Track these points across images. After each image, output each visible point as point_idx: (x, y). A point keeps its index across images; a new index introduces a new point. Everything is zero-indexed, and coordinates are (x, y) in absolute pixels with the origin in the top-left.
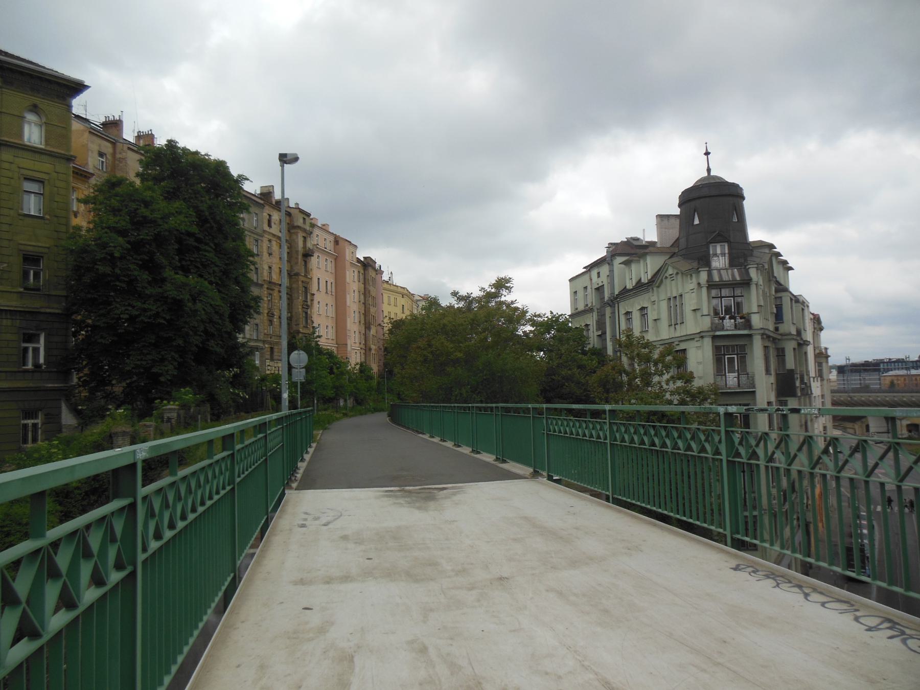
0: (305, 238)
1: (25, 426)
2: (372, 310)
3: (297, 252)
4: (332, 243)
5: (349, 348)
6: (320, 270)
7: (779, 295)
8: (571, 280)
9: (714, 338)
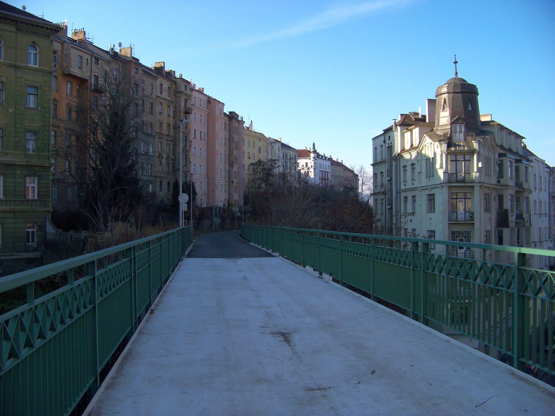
0: (186, 100)
1: (28, 232)
2: (235, 152)
3: (180, 110)
4: (206, 102)
5: (216, 182)
6: (197, 123)
7: (501, 158)
8: (373, 139)
9: (450, 187)
